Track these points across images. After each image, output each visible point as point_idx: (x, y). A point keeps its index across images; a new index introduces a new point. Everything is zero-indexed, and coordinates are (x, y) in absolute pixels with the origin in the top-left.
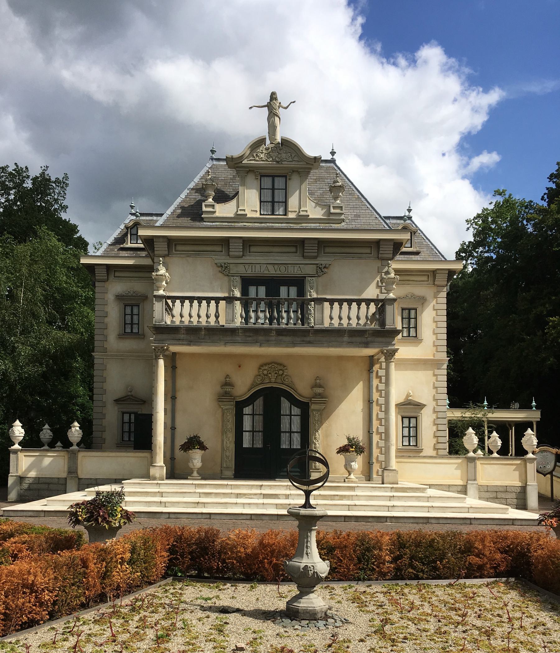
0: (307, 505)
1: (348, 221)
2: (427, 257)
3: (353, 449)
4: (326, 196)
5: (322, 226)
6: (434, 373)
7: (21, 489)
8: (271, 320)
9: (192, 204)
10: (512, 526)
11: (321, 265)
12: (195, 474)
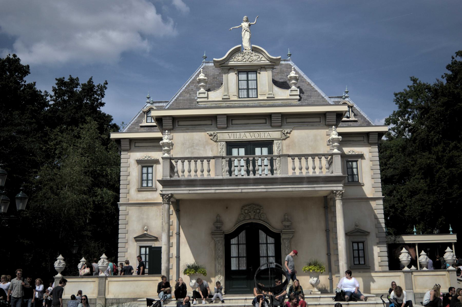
8: (248, 172)
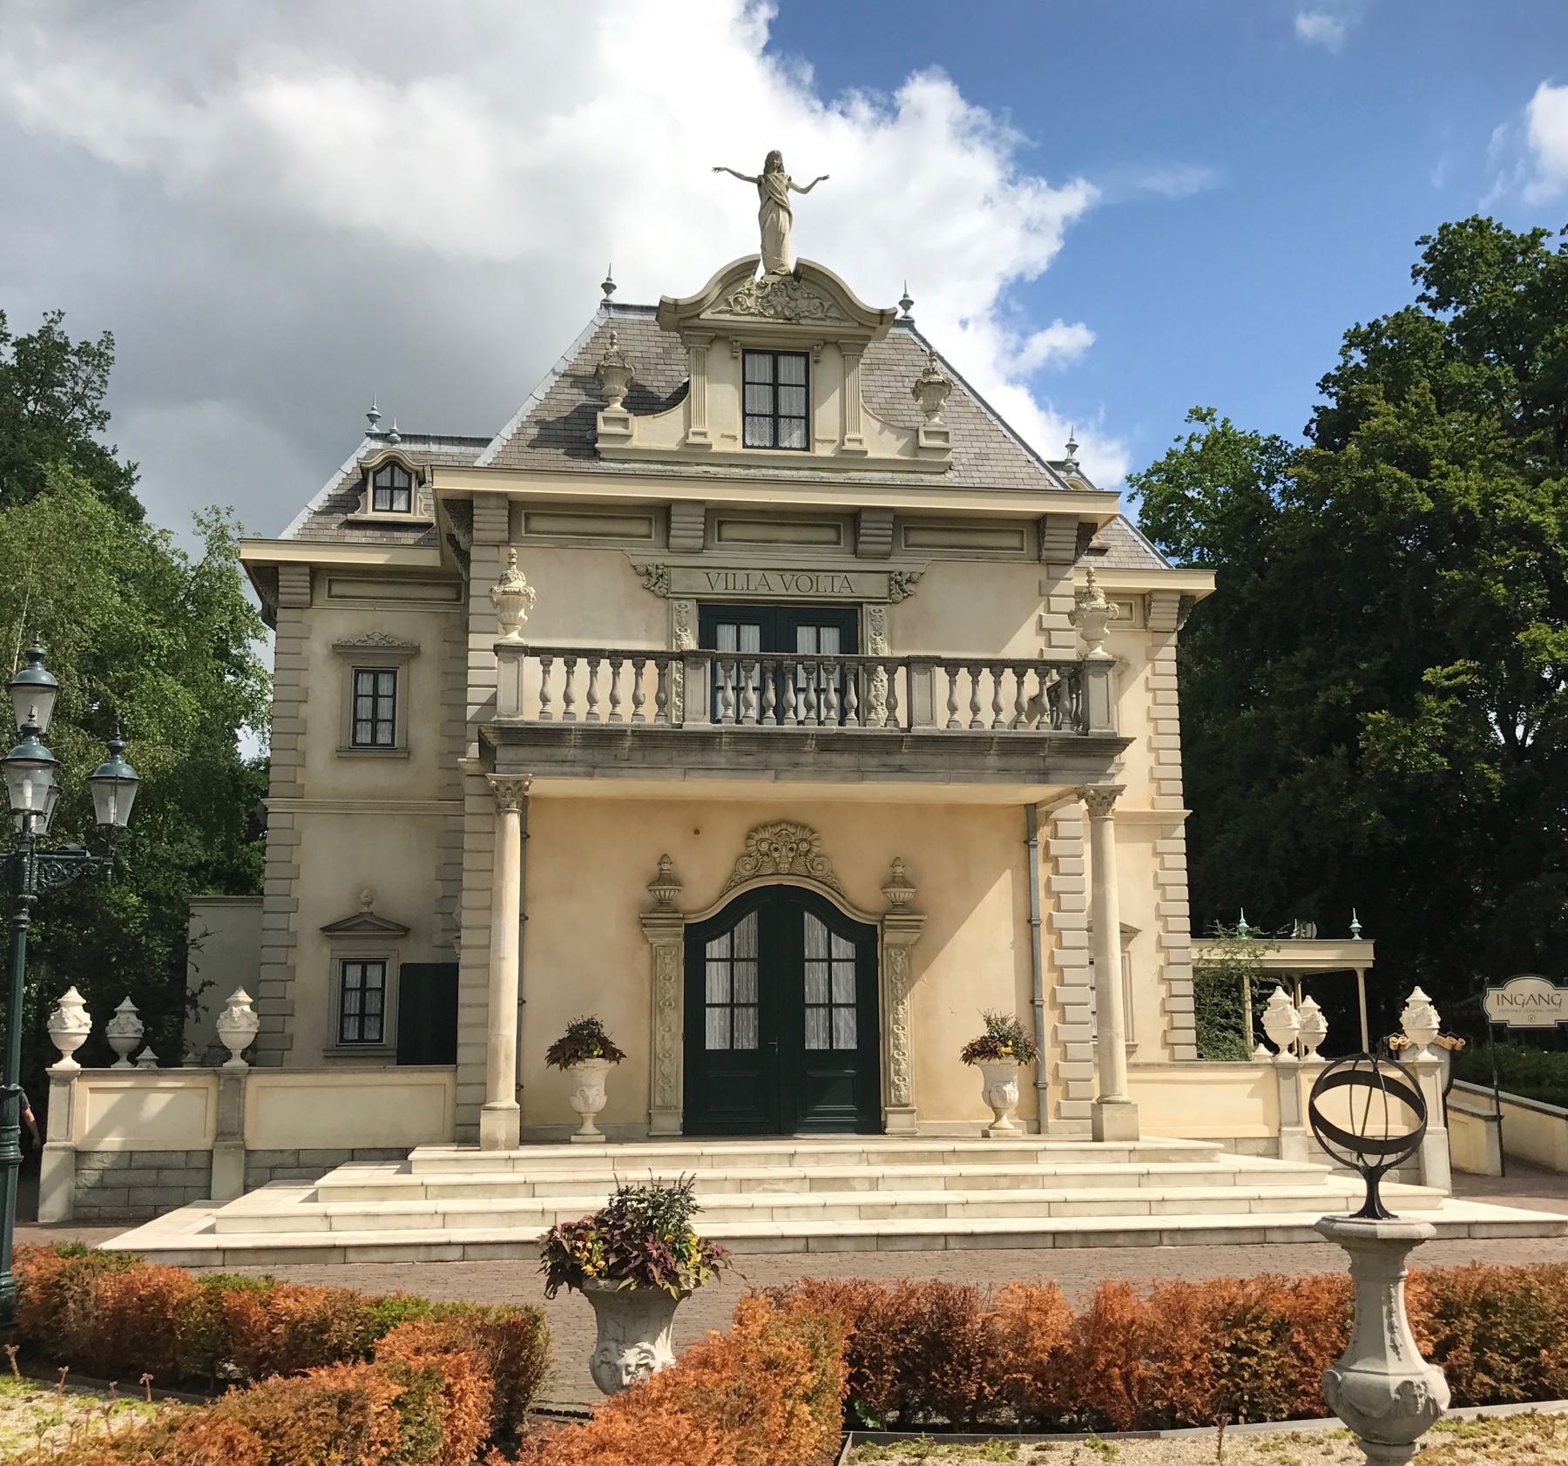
0: (1372, 1208)
1: (961, 468)
2: (1127, 560)
3: (1009, 1050)
4: (901, 407)
5: (900, 478)
6: (1154, 848)
7: (78, 1187)
9: (565, 414)
10: (1469, 1241)
11: (900, 574)
12: (589, 1128)
